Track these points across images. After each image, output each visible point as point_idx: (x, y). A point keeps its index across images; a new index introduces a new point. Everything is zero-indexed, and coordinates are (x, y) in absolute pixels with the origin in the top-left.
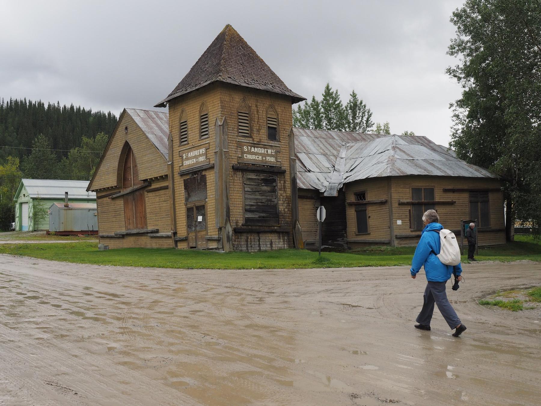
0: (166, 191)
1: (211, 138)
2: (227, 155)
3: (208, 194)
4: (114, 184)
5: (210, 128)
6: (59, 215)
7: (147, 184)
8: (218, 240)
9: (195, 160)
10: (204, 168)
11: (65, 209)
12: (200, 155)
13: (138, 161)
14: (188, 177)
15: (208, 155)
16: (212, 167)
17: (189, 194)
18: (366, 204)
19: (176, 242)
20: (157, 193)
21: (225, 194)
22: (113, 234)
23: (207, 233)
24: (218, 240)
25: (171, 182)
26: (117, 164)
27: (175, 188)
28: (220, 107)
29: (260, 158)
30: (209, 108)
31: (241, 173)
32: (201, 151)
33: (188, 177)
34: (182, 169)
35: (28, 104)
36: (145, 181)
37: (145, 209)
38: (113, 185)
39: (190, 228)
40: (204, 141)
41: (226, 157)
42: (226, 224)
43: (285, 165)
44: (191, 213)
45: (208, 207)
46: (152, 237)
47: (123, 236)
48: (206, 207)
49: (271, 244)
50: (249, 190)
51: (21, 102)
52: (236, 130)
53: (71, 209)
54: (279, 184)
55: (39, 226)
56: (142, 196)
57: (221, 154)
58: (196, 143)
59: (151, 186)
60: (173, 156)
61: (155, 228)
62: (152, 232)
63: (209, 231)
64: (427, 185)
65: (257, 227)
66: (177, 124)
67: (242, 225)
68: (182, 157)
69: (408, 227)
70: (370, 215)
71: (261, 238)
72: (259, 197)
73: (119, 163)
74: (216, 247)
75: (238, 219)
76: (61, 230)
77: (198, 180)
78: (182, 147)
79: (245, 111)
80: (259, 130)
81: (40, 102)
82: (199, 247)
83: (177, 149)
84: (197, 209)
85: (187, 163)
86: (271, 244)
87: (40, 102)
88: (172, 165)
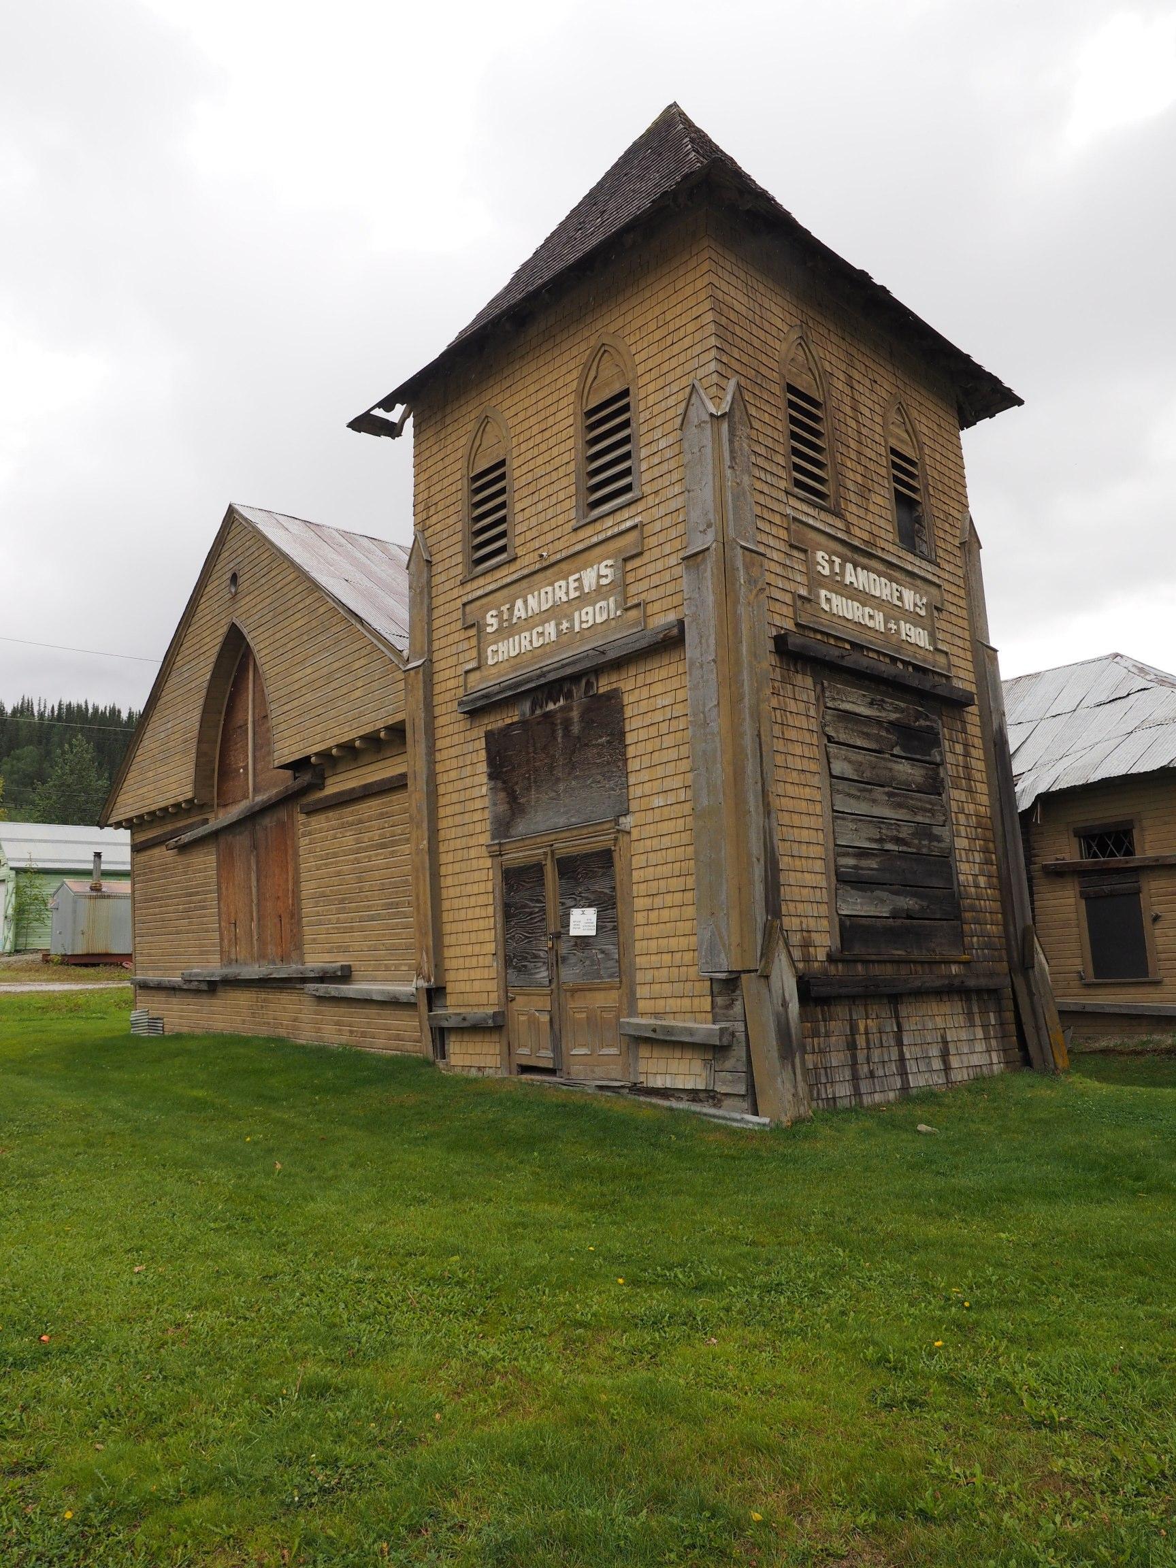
1: (651, 501)
2: (755, 572)
3: (635, 792)
6: (75, 911)
7: (306, 778)
8: (714, 1051)
10: (611, 655)
11: (90, 897)
13: (273, 690)
14: (511, 717)
16: (670, 642)
17: (513, 799)
19: (440, 1035)
20: (349, 814)
21: (742, 792)
22: (176, 979)
23: (632, 999)
24: (714, 1051)
26: (196, 716)
27: (441, 778)
28: (712, 328)
31: (809, 682)
33: (511, 717)
35: (91, 711)
37: (297, 882)
38: (181, 799)
39: (521, 970)
40: (609, 522)
41: (751, 581)
42: (767, 953)
43: (962, 674)
44: (524, 897)
45: (638, 861)
46: (321, 999)
47: (212, 987)
48: (619, 864)
49: (945, 1056)
50: (849, 772)
51: (79, 707)
53: (109, 897)
54: (951, 756)
55: (30, 940)
56: (285, 831)
57: (726, 563)
58: (559, 545)
59: (321, 787)
60: (431, 631)
61: (337, 961)
62: (323, 978)
63: (641, 991)
65: (889, 969)
66: (455, 487)
67: (831, 958)
70: (1157, 909)
71: (906, 1027)
72: (887, 812)
73: (205, 712)
75: (812, 923)
76: (80, 952)
77: (567, 723)
80: (864, 492)
81: (114, 708)
82: (577, 1071)
83: (450, 594)
84: (562, 874)
85: (502, 652)
86: (945, 1056)
87: (114, 708)
88: (428, 671)
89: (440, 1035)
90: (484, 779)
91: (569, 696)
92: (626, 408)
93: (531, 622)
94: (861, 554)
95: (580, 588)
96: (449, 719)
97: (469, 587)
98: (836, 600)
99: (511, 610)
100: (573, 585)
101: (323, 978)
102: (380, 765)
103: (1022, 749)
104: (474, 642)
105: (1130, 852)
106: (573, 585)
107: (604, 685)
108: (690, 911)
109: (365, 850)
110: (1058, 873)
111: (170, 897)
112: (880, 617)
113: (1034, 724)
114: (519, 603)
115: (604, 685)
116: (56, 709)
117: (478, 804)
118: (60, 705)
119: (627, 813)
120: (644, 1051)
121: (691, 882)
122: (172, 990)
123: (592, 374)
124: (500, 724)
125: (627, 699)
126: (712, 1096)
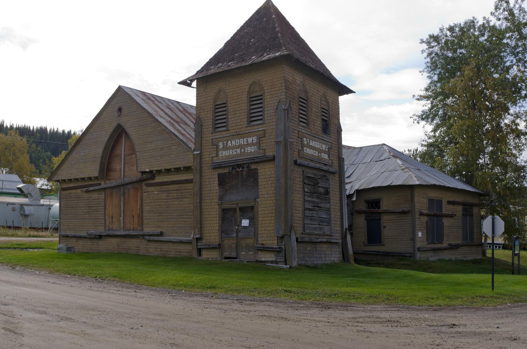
0: (190, 186)
4: (96, 174)
8: (277, 251)
9: (239, 150)
14: (226, 170)
15: (262, 145)
18: (380, 213)
22: (84, 234)
23: (257, 240)
28: (284, 87)
34: (215, 160)
40: (256, 127)
41: (291, 148)
44: (228, 216)
46: (149, 241)
59: (154, 179)
64: (438, 196)
68: (217, 146)
69: (425, 240)
70: (385, 224)
83: (208, 135)
84: (240, 211)
85: (223, 154)
90: (217, 185)
91: (243, 168)
93: (232, 148)
94: (314, 137)
95: (247, 142)
97: (214, 135)
98: (308, 150)
99: (227, 143)
100: (245, 141)
102: (178, 176)
103: (353, 174)
104: (215, 149)
105: (379, 208)
106: (245, 141)
108: (273, 222)
109: (170, 199)
110: (360, 212)
112: (317, 153)
113: (357, 165)
114: (229, 142)
115: (253, 167)
117: (215, 191)
119: (258, 198)
120: (260, 253)
121: (273, 215)
123: (252, 88)
124: (222, 172)
126: (276, 262)
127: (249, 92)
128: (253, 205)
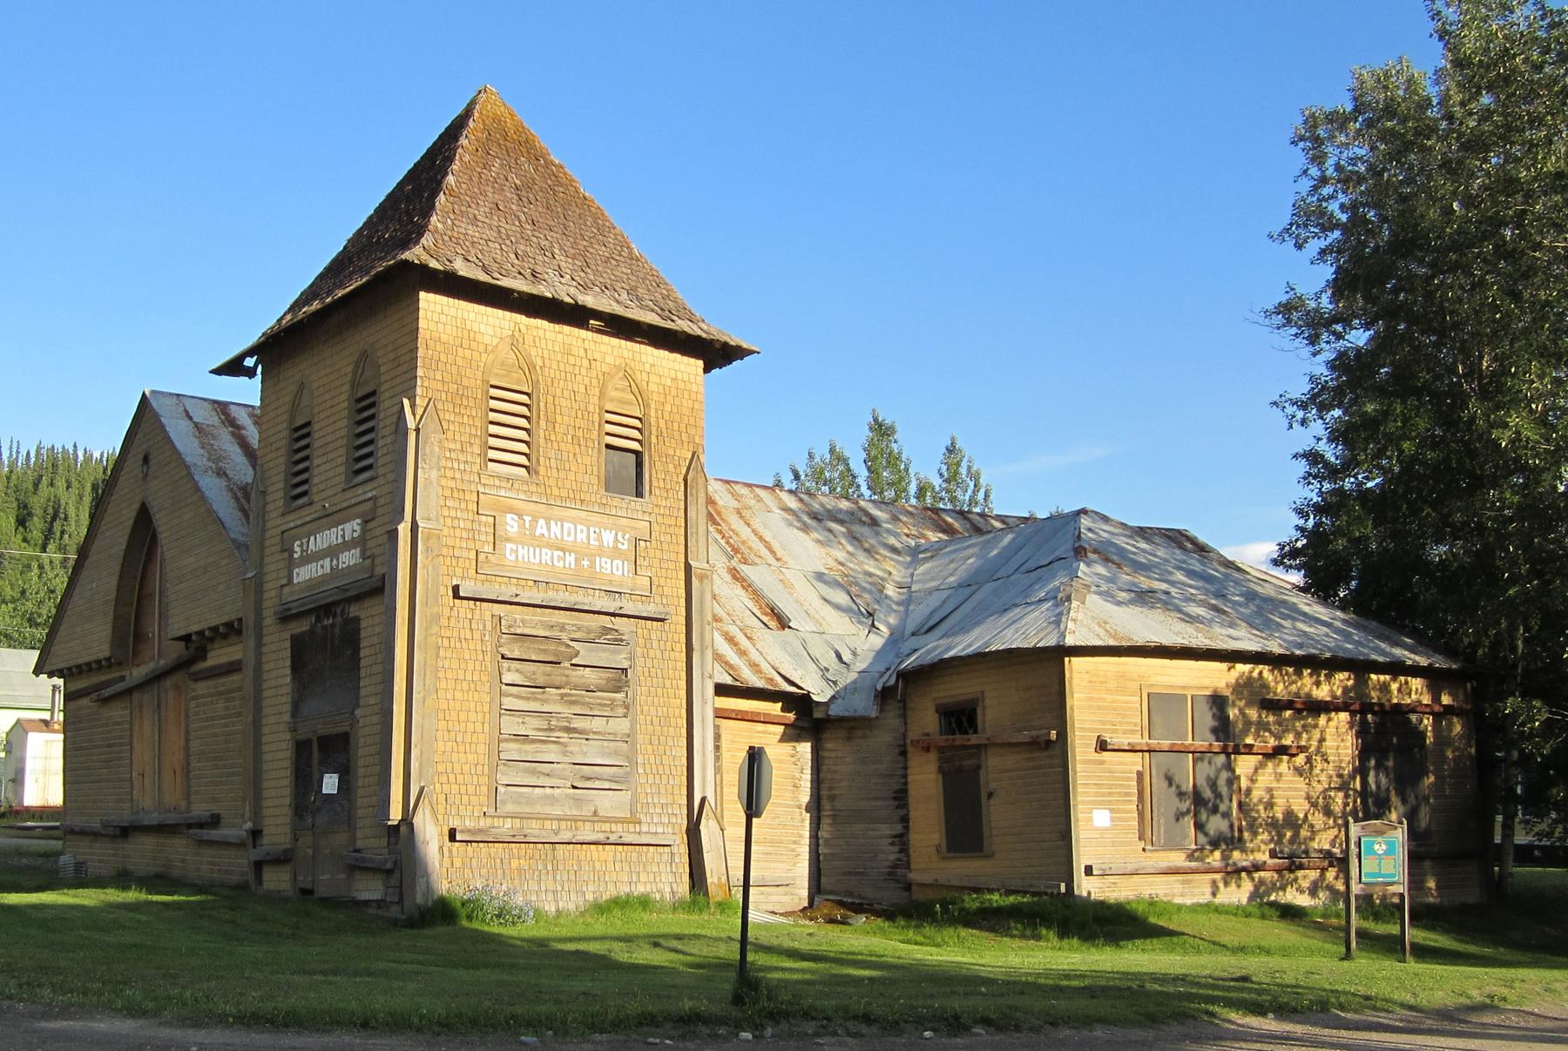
1: (381, 480)
5: (380, 443)
12: (346, 546)
18: (978, 747)
22: (96, 825)
25: (251, 643)
26: (114, 582)
27: (266, 667)
29: (571, 559)
30: (383, 369)
32: (348, 527)
36: (186, 638)
38: (101, 656)
45: (361, 741)
50: (518, 679)
52: (477, 450)
59: (204, 658)
63: (359, 834)
68: (292, 552)
70: (993, 786)
74: (376, 896)
78: (293, 516)
79: (519, 381)
83: (276, 522)
85: (303, 574)
89: (258, 866)
92: (373, 405)
96: (269, 620)
101: (201, 826)
107: (354, 610)
111: (96, 747)
116: (33, 455)
118: (39, 449)
120: (358, 875)
122: (94, 835)
125: (363, 624)
127: (354, 385)
128: (347, 729)
